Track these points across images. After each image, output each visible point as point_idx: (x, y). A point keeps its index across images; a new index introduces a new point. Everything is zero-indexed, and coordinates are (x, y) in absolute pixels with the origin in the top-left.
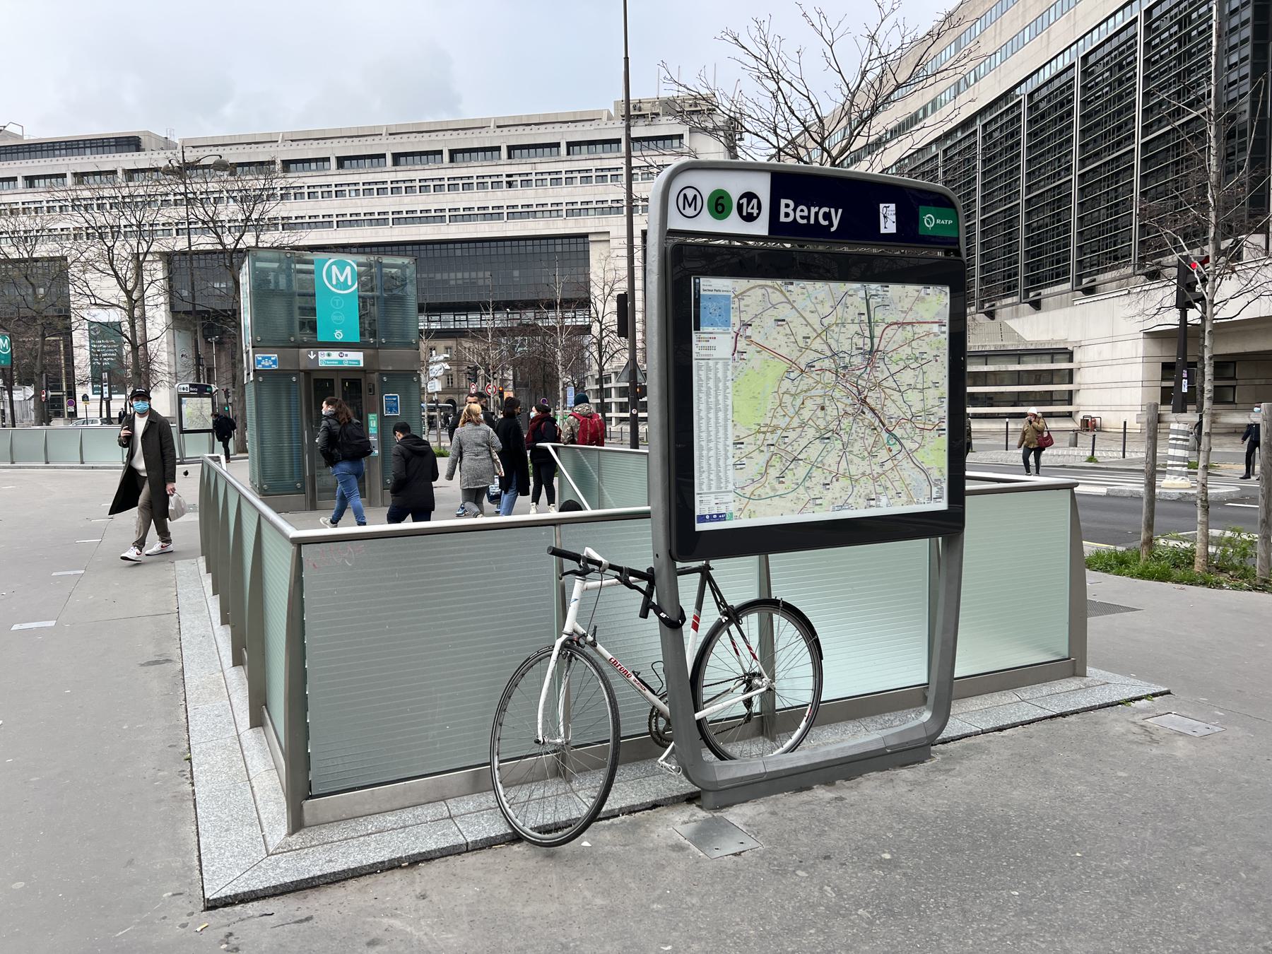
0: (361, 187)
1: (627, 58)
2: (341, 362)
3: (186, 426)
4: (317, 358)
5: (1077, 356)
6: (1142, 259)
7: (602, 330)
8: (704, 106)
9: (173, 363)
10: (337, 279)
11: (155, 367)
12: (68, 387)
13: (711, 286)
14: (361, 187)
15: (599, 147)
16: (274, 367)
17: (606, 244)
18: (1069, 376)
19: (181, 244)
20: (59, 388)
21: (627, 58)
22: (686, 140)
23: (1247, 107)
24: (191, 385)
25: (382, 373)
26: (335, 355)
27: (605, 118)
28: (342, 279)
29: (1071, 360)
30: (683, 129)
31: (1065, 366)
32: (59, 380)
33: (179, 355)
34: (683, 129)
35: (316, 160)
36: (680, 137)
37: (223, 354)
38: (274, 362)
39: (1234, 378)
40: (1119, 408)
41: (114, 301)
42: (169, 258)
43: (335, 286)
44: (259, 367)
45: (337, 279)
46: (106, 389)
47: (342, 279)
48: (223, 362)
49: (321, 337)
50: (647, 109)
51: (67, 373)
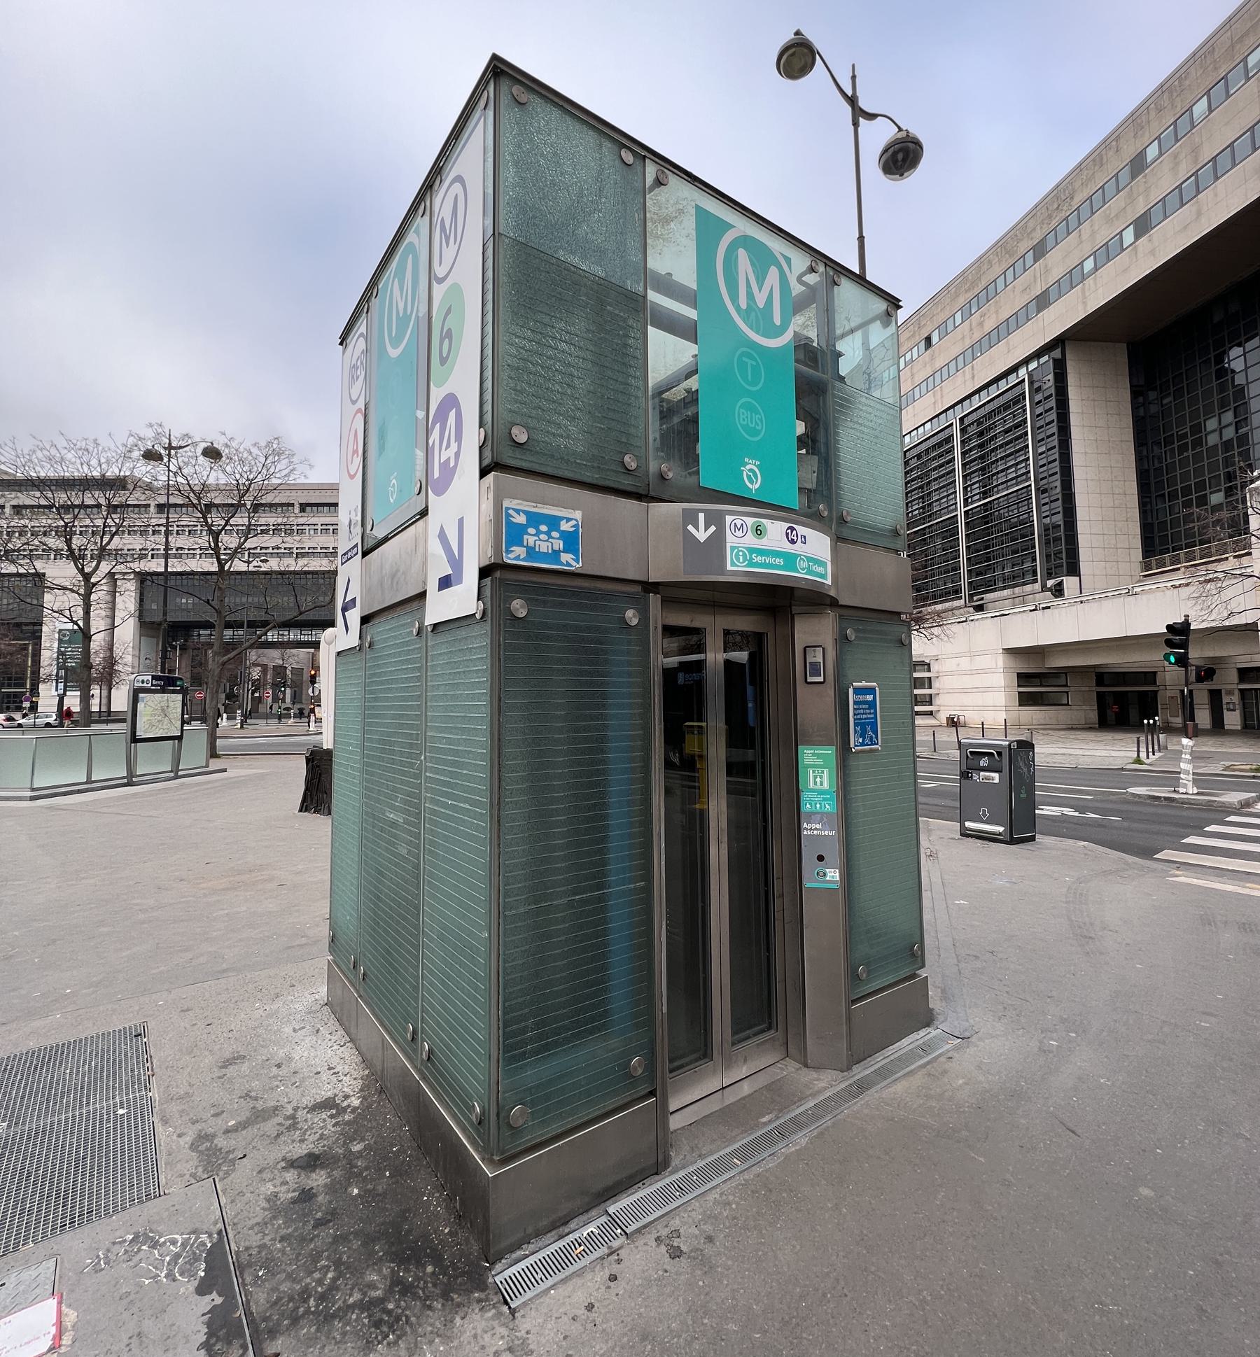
0: (319, 527)
1: (861, 238)
2: (791, 559)
3: (141, 733)
4: (718, 540)
5: (934, 667)
6: (971, 596)
9: (136, 664)
11: (118, 667)
12: (32, 685)
13: (141, 695)
14: (319, 527)
16: (569, 561)
18: (928, 683)
19: (156, 566)
20: (23, 685)
21: (861, 238)
23: (1058, 484)
24: (154, 678)
28: (761, 300)
29: (929, 670)
31: (926, 674)
32: (24, 678)
33: (143, 658)
35: (282, 505)
37: (185, 656)
38: (570, 541)
39: (1066, 686)
40: (984, 708)
41: (67, 584)
42: (143, 578)
43: (746, 315)
44: (515, 556)
45: (750, 295)
46: (61, 686)
47: (761, 300)
48: (183, 665)
49: (709, 477)
51: (33, 673)
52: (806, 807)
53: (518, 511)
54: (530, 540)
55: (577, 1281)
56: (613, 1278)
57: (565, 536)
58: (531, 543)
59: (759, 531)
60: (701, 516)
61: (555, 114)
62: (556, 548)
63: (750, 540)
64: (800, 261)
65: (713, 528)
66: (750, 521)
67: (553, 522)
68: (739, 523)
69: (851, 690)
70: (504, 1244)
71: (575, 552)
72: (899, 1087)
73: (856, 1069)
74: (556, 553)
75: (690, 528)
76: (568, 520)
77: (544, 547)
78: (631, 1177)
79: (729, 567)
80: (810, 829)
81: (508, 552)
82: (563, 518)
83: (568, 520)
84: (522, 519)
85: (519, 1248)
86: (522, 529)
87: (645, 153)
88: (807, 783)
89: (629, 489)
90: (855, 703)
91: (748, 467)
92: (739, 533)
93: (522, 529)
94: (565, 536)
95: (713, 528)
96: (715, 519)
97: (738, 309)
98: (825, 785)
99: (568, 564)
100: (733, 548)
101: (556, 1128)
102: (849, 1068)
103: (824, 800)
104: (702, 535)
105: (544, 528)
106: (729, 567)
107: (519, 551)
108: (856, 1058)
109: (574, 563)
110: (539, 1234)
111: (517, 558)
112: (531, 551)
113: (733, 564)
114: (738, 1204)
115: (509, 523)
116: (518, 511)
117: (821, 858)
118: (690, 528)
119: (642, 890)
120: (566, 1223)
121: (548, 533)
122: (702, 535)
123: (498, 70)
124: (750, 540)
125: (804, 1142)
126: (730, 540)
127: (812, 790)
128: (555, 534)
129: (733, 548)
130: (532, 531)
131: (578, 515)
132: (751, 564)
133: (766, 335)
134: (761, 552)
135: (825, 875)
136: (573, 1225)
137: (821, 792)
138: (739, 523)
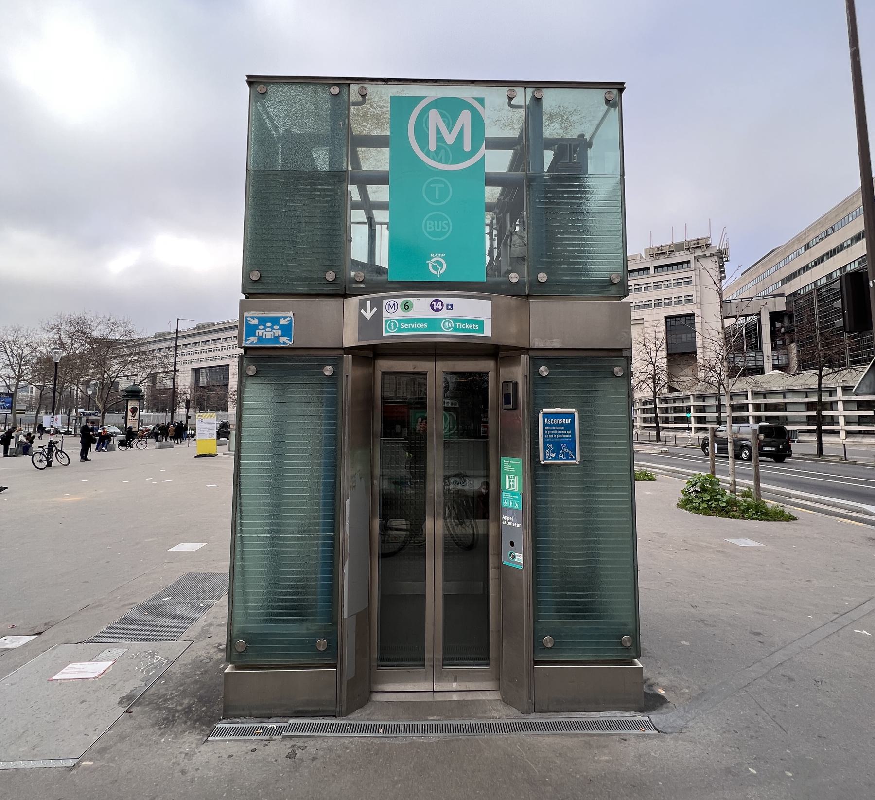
2: (433, 323)
4: (378, 316)
7: (655, 370)
8: (702, 243)
10: (440, 138)
15: (637, 273)
16: (285, 341)
17: (641, 326)
22: (692, 265)
25: (539, 356)
26: (421, 306)
27: (639, 258)
28: (450, 139)
30: (691, 257)
34: (691, 257)
36: (688, 262)
38: (286, 330)
43: (436, 156)
45: (440, 138)
47: (450, 139)
50: (666, 249)
52: (504, 504)
53: (253, 318)
54: (260, 333)
55: (241, 743)
56: (254, 751)
57: (282, 327)
58: (261, 334)
59: (406, 307)
60: (369, 302)
61: (286, 88)
62: (277, 334)
63: (400, 314)
64: (496, 98)
65: (375, 309)
66: (400, 301)
67: (275, 321)
68: (392, 303)
69: (541, 416)
70: (233, 713)
71: (289, 336)
72: (548, 740)
73: (533, 715)
74: (276, 338)
75: (363, 311)
76: (285, 318)
77: (269, 335)
78: (315, 711)
79: (384, 334)
80: (507, 520)
81: (246, 340)
82: (281, 317)
83: (285, 318)
84: (255, 322)
85: (239, 718)
86: (256, 327)
87: (343, 83)
88: (505, 485)
89: (331, 292)
90: (545, 425)
91: (433, 260)
92: (391, 310)
93: (256, 327)
94: (282, 327)
95: (375, 309)
96: (377, 303)
97: (428, 153)
98: (516, 488)
99: (284, 343)
100: (387, 321)
101: (265, 661)
102: (528, 713)
103: (515, 499)
104: (368, 315)
105: (269, 325)
106: (384, 334)
107: (253, 339)
108: (535, 708)
109: (288, 342)
110: (251, 716)
111: (252, 343)
112: (261, 339)
113: (387, 331)
114: (352, 751)
115: (248, 325)
116: (253, 318)
117: (512, 544)
118: (363, 311)
119: (333, 538)
120: (270, 718)
121: (272, 327)
122: (368, 315)
123: (253, 81)
124: (400, 314)
125: (432, 740)
126: (385, 315)
127: (508, 491)
128: (276, 327)
129: (387, 321)
130: (261, 327)
131: (291, 314)
132: (400, 330)
133: (456, 161)
134: (407, 321)
135: (514, 558)
136: (270, 720)
137: (513, 493)
138: (392, 303)
